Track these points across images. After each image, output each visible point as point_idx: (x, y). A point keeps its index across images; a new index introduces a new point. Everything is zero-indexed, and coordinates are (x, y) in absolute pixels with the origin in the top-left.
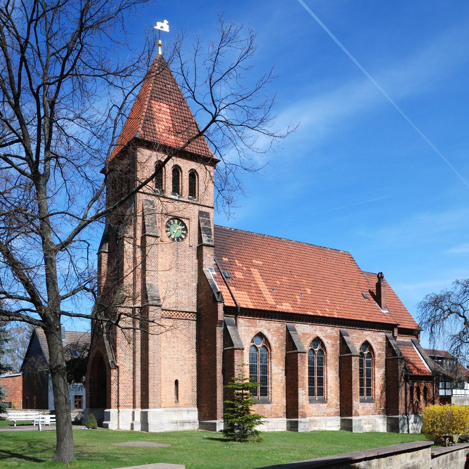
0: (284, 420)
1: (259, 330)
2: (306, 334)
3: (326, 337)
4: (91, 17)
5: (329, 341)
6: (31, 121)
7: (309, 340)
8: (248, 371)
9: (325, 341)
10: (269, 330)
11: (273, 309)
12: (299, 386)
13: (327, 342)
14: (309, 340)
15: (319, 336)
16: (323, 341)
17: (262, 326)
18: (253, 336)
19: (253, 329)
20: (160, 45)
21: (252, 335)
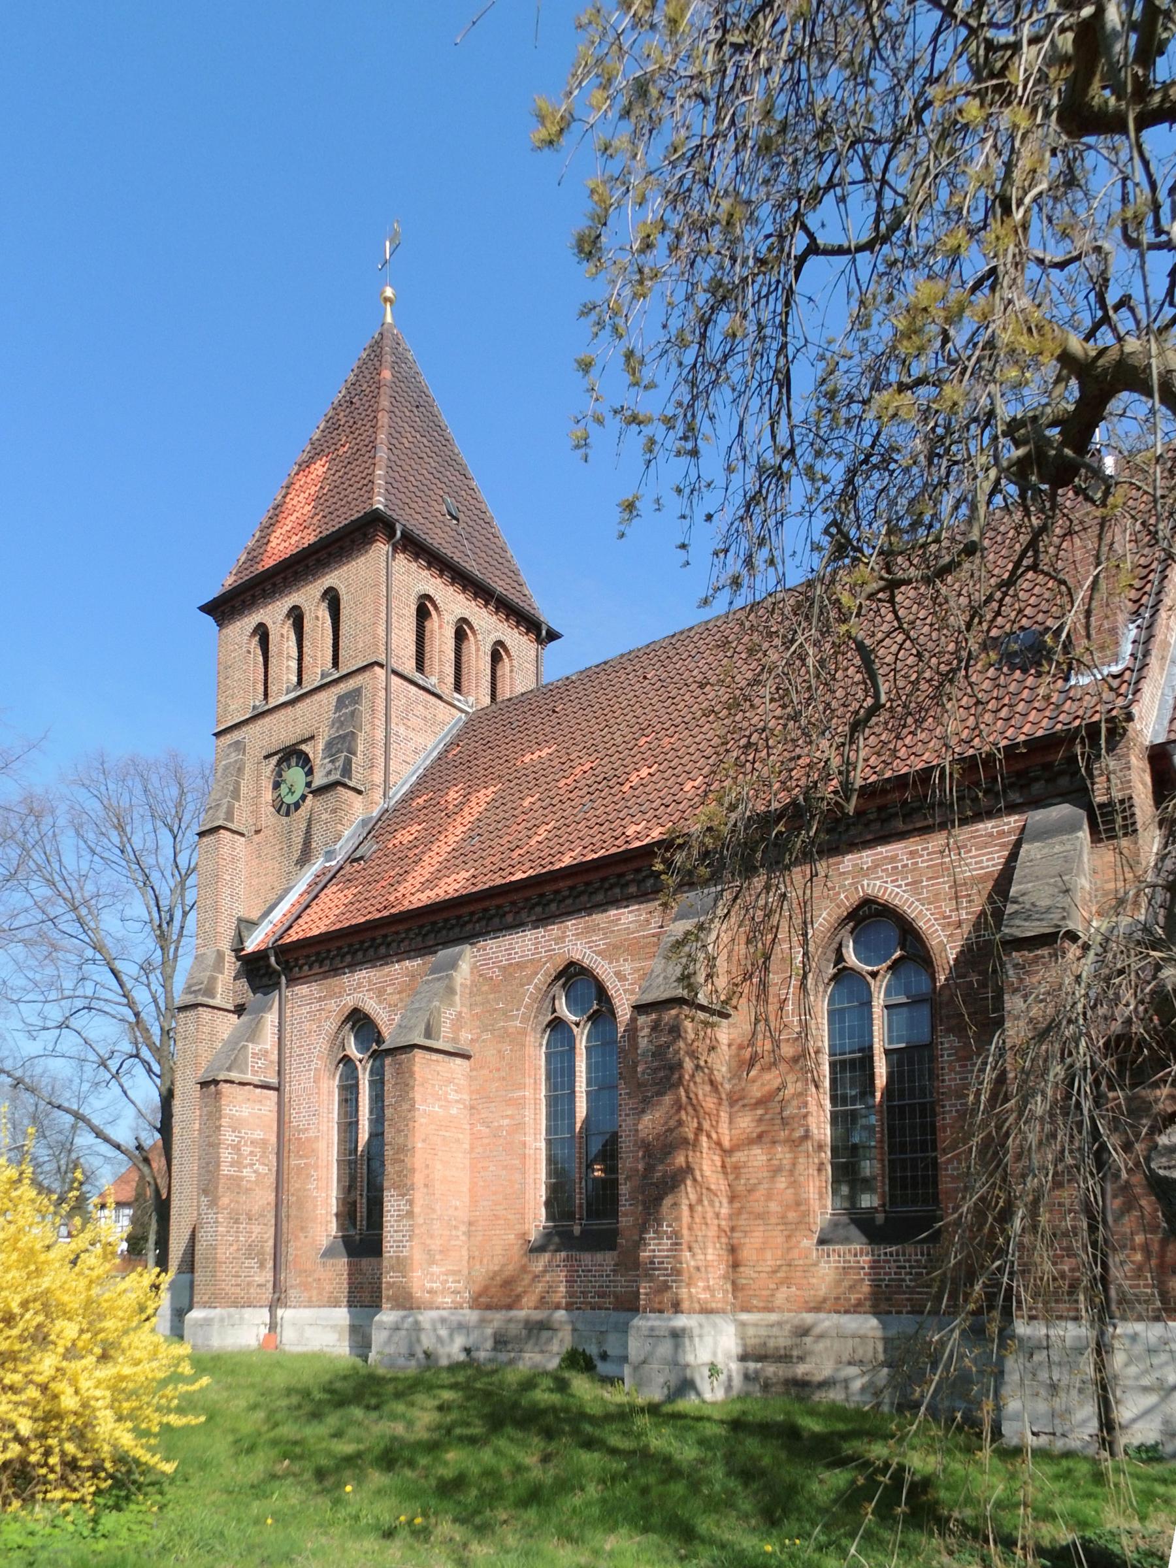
0: (342, 1315)
1: (350, 1001)
2: (520, 966)
3: (610, 953)
4: (884, 182)
5: (627, 968)
6: (897, 618)
7: (531, 988)
8: (623, 1200)
9: (604, 970)
10: (381, 992)
11: (386, 913)
12: (386, 1184)
13: (617, 974)
14: (531, 988)
15: (577, 957)
16: (598, 971)
17: (360, 985)
18: (335, 1027)
19: (332, 1004)
20: (386, 299)
21: (331, 1025)
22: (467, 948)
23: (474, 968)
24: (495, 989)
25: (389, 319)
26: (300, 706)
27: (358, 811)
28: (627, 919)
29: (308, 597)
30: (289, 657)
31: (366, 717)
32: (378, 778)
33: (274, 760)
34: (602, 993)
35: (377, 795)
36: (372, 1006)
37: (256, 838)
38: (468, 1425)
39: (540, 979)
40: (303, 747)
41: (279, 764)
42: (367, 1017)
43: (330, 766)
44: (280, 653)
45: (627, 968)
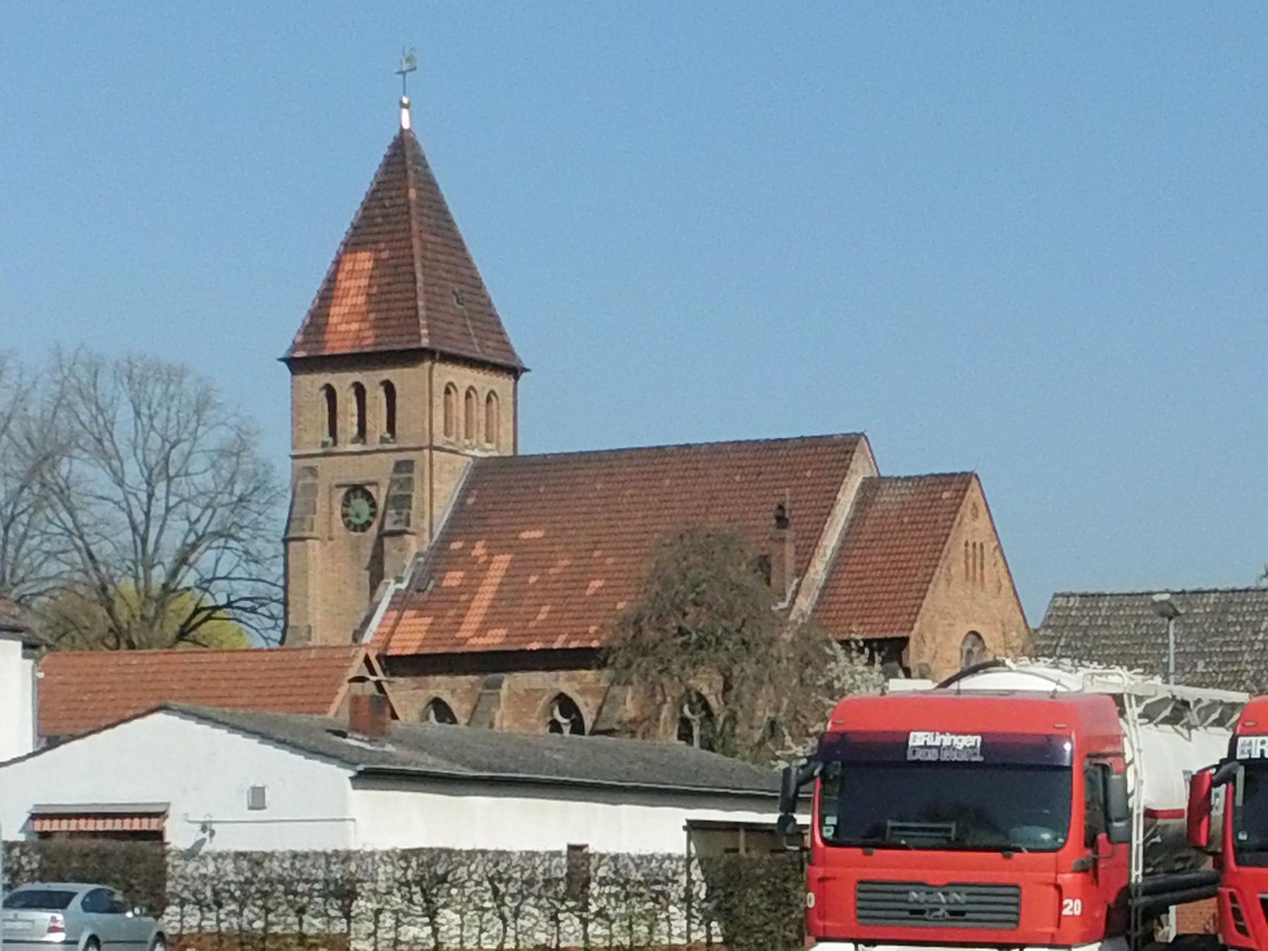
1: (433, 693)
2: (536, 690)
3: (582, 692)
9: (579, 701)
10: (453, 692)
15: (564, 691)
18: (423, 706)
21: (421, 705)
22: (505, 675)
23: (509, 687)
24: (522, 699)
25: (538, 534)
26: (364, 457)
27: (415, 545)
28: (589, 675)
29: (372, 379)
30: (352, 415)
31: (417, 483)
32: (426, 525)
33: (344, 490)
34: (575, 709)
35: (426, 537)
36: (446, 698)
37: (330, 543)
38: (1167, 664)
39: (545, 698)
40: (368, 488)
41: (347, 494)
42: (444, 703)
43: (396, 517)
44: (345, 413)
45: (589, 701)
